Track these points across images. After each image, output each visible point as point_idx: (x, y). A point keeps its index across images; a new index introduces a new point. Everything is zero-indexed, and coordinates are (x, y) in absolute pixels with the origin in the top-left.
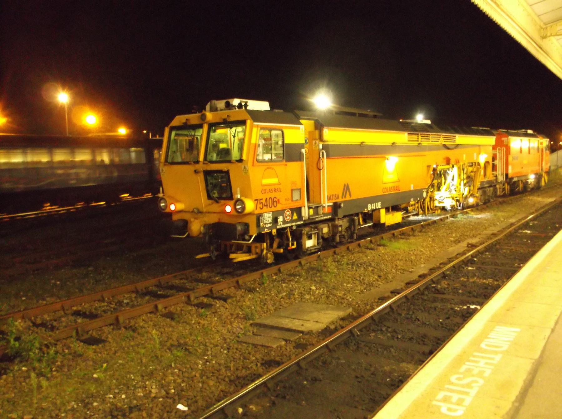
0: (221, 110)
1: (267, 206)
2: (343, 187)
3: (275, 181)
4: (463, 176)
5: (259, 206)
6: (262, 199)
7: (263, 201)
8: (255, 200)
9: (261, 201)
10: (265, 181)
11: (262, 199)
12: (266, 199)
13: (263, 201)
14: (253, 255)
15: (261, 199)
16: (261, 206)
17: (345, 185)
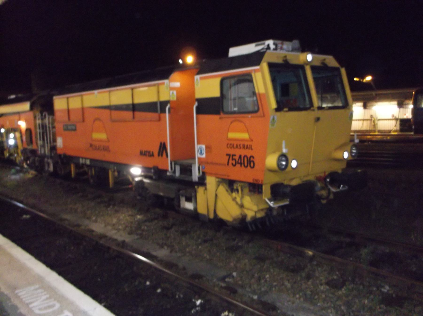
1: (241, 164)
3: (245, 136)
5: (231, 162)
6: (235, 155)
9: (234, 157)
10: (231, 135)
11: (235, 155)
13: (237, 158)
16: (234, 162)
17: (161, 143)
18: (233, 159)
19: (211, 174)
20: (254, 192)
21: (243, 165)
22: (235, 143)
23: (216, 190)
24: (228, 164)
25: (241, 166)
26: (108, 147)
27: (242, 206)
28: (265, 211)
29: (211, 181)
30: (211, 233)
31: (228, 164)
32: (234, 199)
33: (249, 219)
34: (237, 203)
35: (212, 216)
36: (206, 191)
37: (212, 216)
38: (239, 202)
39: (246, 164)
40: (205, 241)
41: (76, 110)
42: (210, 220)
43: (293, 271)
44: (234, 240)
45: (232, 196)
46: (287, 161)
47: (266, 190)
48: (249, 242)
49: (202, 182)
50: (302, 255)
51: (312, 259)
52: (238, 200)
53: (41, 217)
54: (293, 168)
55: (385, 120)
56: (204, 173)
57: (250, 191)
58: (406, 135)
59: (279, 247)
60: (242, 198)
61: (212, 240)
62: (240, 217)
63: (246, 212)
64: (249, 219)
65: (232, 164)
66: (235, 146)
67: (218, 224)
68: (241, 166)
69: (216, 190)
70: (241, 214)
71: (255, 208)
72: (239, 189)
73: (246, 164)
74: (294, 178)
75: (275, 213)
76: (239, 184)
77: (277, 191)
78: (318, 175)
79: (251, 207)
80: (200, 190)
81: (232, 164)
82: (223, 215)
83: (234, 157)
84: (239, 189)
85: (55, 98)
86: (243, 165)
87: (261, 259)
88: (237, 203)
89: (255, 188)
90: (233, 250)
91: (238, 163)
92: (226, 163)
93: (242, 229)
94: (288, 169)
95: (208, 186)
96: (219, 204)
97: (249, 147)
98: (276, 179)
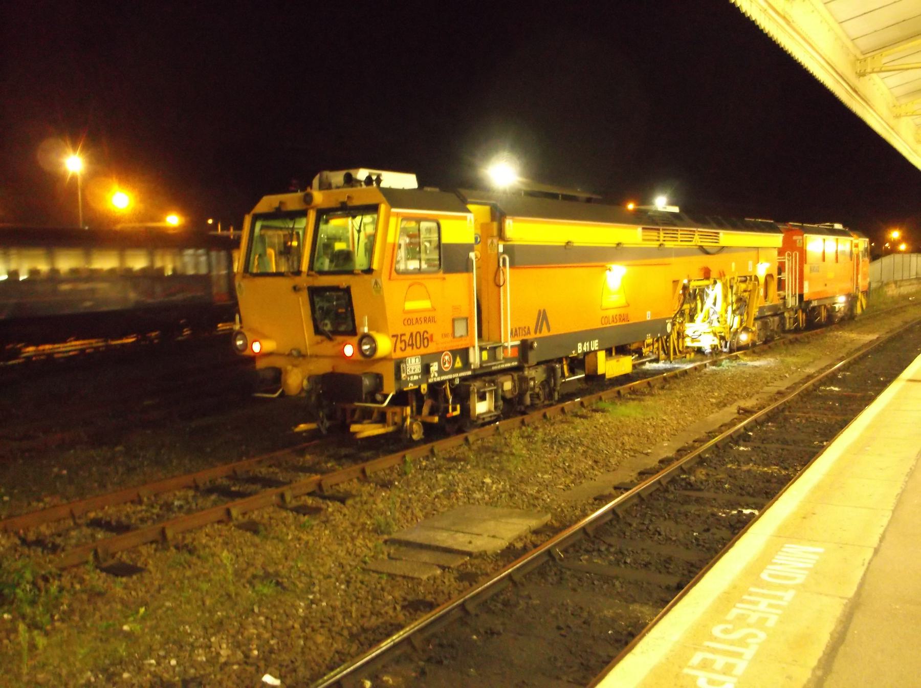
0: (338, 187)
1: (412, 345)
2: (537, 313)
3: (425, 304)
4: (732, 298)
5: (399, 345)
6: (404, 335)
7: (407, 338)
8: (393, 336)
9: (403, 338)
10: (410, 305)
11: (404, 335)
12: (412, 334)
13: (407, 338)
14: (388, 426)
15: (401, 335)
16: (403, 346)
17: (540, 312)
18: (401, 341)
22: (414, 316)
26: (627, 315)
41: (843, 253)
46: (362, 352)
55: (908, 69)
58: (271, 261)
59: (133, 593)
66: (414, 321)
83: (403, 338)
85: (867, 240)
97: (431, 320)
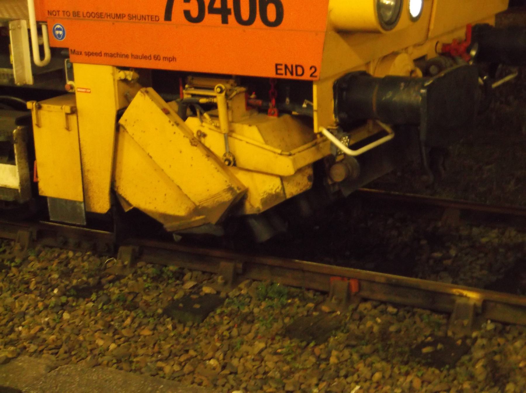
1: (224, 12)
19: (93, 56)
20: (263, 110)
21: (232, 18)
23: (119, 115)
24: (168, 16)
25: (225, 21)
27: (230, 163)
28: (310, 171)
29: (94, 82)
30: (84, 263)
31: (168, 16)
32: (198, 140)
33: (255, 203)
34: (209, 153)
35: (102, 204)
36: (73, 118)
37: (102, 204)
38: (219, 149)
39: (245, 15)
40: (82, 292)
42: (94, 219)
43: (436, 361)
44: (179, 276)
45: (184, 129)
47: (322, 102)
48: (236, 279)
49: (53, 83)
50: (440, 306)
51: (480, 313)
52: (215, 142)
53: (307, 261)
54: (414, 20)
56: (59, 53)
57: (249, 106)
60: (229, 135)
61: (99, 286)
62: (228, 197)
63: (245, 179)
64: (255, 203)
65: (187, 14)
67: (126, 227)
68: (225, 21)
69: (119, 115)
70: (230, 189)
71: (285, 166)
72: (220, 100)
73: (245, 15)
74: (395, 54)
75: (339, 174)
76: (219, 86)
77: (355, 103)
78: (448, 39)
79: (266, 164)
80: (48, 119)
81: (187, 14)
82: (145, 195)
84: (220, 100)
86: (232, 18)
87: (310, 333)
88: (209, 153)
89: (275, 96)
90: (197, 310)
91: (212, 10)
92: (162, 13)
93: (233, 235)
94: (403, 23)
95: (82, 100)
96: (130, 158)
98: (348, 59)
